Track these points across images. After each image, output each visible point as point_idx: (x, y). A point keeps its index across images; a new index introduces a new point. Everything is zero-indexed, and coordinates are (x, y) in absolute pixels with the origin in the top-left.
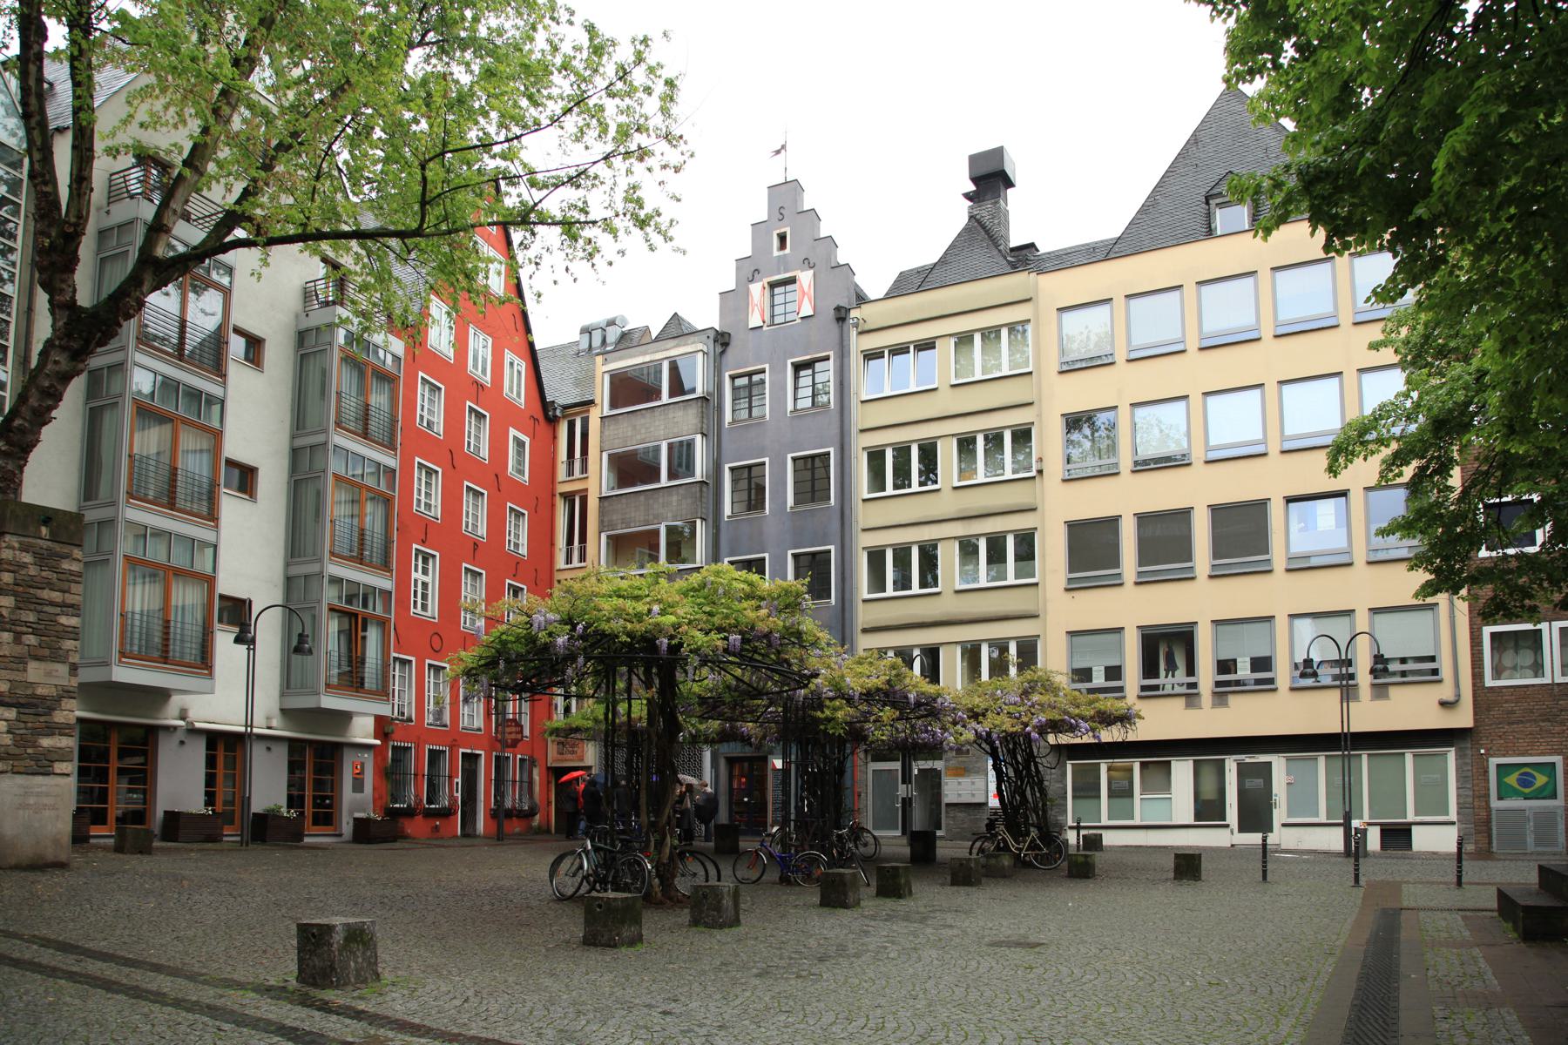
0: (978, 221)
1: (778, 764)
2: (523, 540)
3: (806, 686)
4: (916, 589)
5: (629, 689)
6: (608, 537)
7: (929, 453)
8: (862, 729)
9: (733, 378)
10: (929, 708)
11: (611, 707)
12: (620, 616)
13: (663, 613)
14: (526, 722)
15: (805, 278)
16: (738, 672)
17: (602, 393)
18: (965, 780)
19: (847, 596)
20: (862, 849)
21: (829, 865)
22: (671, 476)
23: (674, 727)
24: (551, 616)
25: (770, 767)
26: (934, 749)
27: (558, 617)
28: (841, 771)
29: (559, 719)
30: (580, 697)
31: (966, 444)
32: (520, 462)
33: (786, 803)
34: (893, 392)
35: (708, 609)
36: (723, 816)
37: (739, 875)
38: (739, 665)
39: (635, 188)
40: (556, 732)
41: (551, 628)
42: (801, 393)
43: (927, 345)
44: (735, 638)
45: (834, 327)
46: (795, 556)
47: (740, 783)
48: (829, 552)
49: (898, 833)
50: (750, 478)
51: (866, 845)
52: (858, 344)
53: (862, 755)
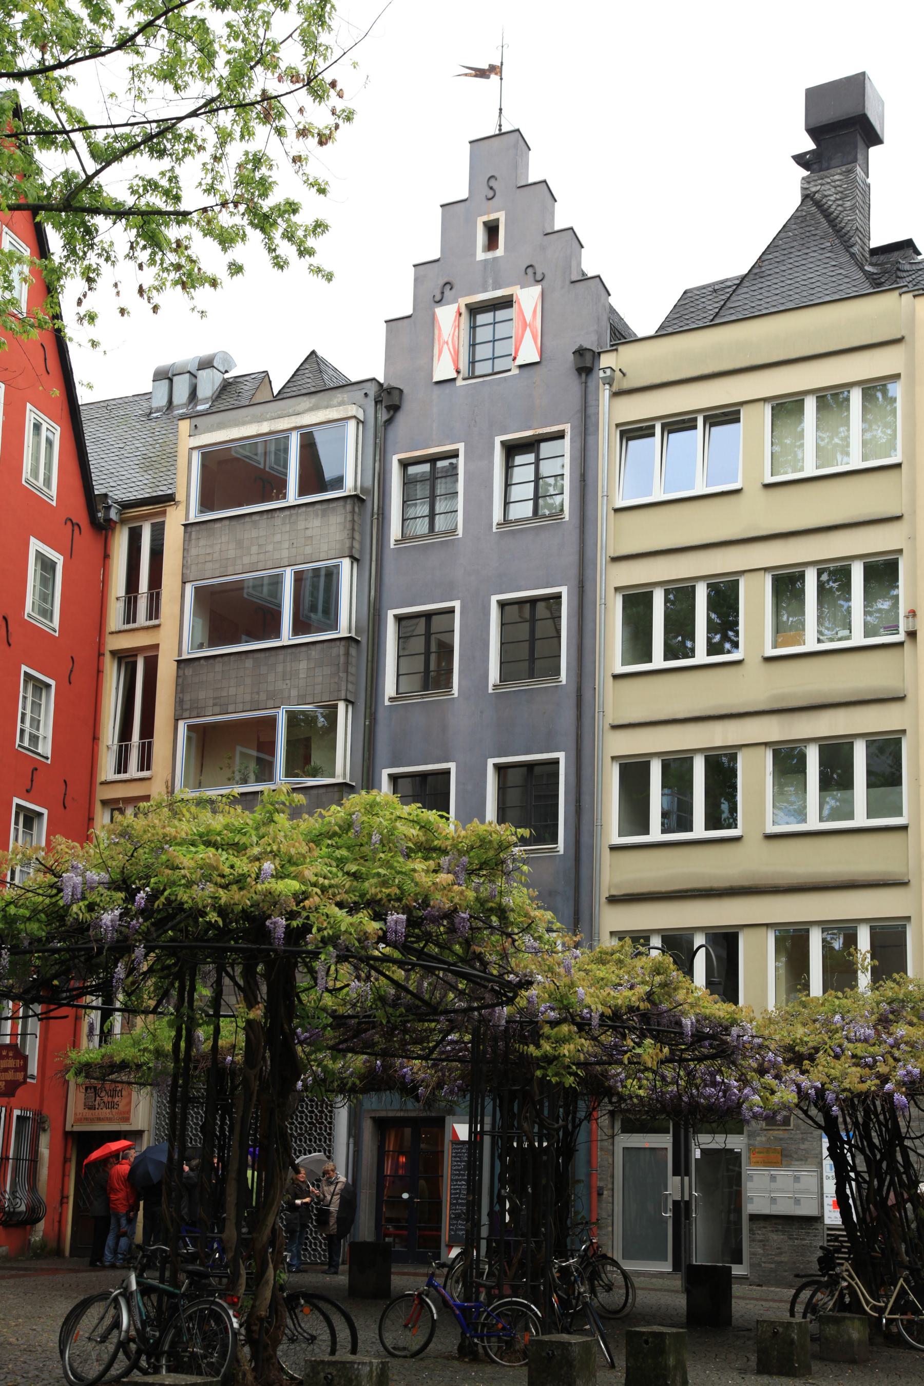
0: (818, 204)
1: (462, 1131)
2: (47, 731)
3: (510, 1001)
4: (699, 831)
5: (216, 1001)
6: (190, 728)
7: (725, 598)
8: (605, 1075)
9: (405, 465)
10: (716, 1044)
11: (185, 1025)
12: (208, 879)
13: (279, 876)
14: (33, 1049)
15: (528, 298)
16: (399, 974)
17: (188, 483)
18: (780, 1173)
19: (585, 839)
20: (602, 1296)
21: (546, 1326)
22: (300, 627)
23: (290, 1067)
24: (94, 875)
25: (448, 1137)
26: (728, 1117)
27: (104, 876)
28: (568, 1149)
29: (90, 1049)
30: (130, 1011)
31: (787, 585)
32: (46, 597)
33: (474, 1206)
34: (667, 494)
35: (353, 868)
36: (365, 1228)
37: (389, 1343)
38: (400, 964)
39: (257, 160)
40: (85, 1069)
41: (93, 897)
42: (516, 493)
43: (726, 416)
44: (396, 918)
45: (573, 384)
46: (499, 768)
47: (396, 1165)
48: (556, 762)
49: (667, 1267)
50: (428, 634)
51: (609, 1288)
52: (613, 412)
53: (605, 1121)
